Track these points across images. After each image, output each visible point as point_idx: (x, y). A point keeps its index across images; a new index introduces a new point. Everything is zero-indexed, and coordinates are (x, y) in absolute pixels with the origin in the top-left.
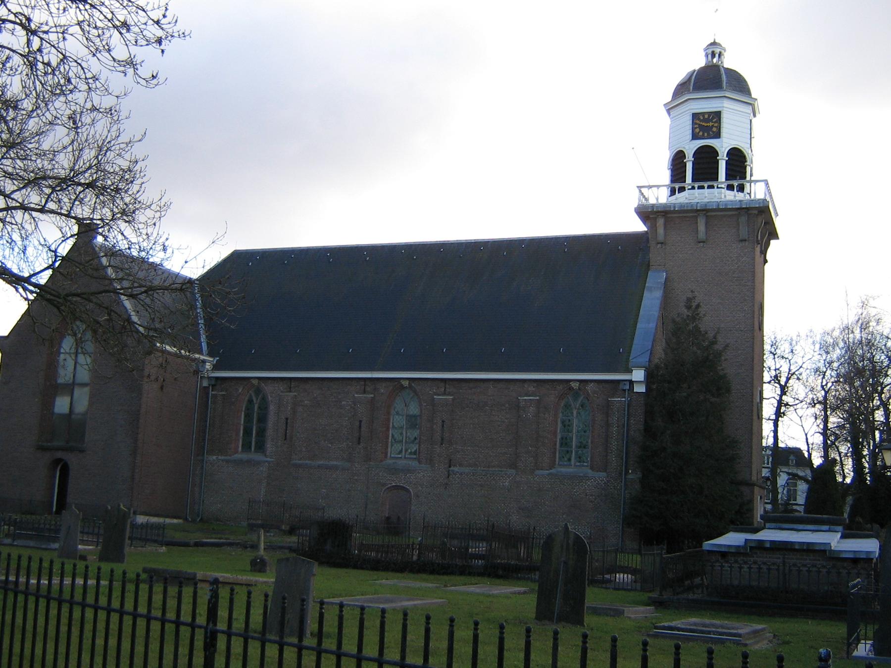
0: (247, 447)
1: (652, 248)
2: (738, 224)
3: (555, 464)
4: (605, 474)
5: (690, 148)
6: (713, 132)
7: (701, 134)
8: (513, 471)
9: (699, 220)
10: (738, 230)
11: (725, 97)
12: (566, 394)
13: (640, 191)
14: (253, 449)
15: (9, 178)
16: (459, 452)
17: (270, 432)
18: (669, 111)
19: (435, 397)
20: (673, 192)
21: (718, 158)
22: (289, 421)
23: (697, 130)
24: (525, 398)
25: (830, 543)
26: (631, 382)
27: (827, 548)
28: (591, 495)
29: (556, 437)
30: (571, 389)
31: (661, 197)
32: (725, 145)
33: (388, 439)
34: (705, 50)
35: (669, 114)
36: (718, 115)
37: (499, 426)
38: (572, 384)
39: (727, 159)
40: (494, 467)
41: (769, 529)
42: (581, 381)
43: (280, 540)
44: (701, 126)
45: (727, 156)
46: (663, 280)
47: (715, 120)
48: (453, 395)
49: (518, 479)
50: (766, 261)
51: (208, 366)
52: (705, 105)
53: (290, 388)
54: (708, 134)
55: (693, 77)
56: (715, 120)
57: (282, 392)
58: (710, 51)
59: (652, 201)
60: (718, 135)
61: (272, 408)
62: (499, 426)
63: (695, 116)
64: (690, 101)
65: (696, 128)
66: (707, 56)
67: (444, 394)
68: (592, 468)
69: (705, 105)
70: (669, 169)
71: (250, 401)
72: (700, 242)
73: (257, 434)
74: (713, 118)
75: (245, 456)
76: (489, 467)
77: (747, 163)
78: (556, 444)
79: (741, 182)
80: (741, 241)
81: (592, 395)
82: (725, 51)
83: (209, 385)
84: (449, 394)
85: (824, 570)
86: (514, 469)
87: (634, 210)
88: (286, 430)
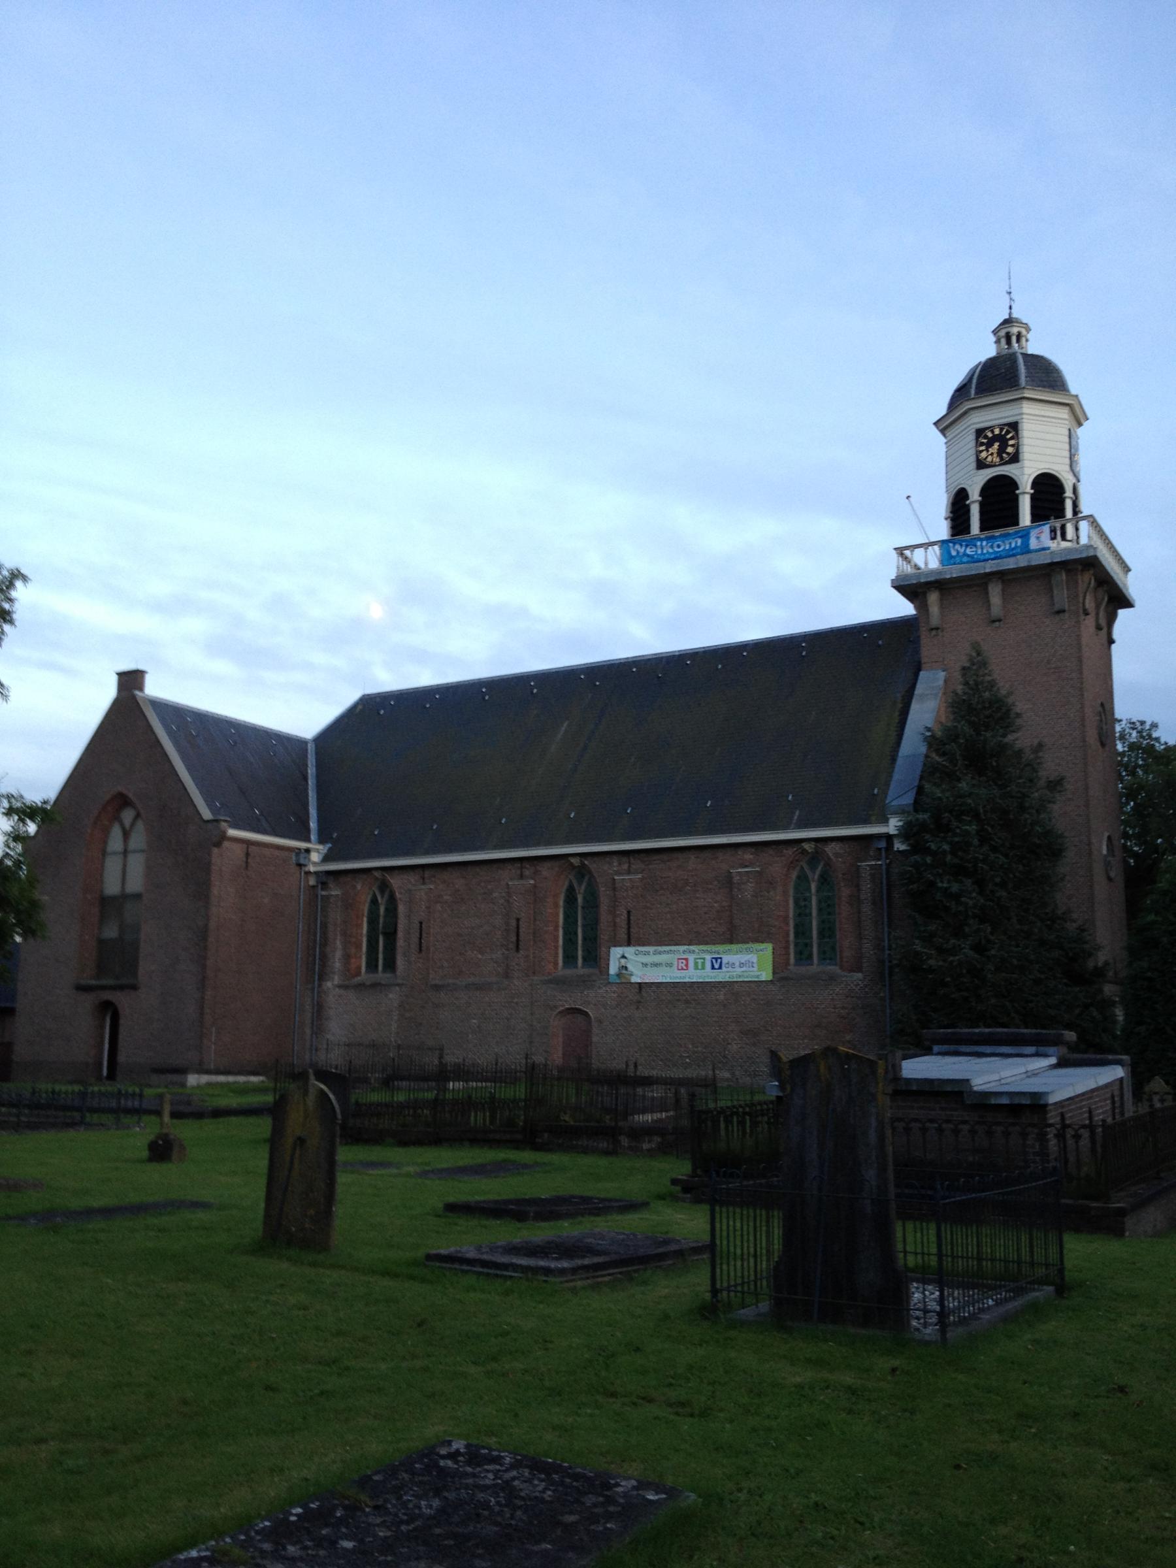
0: (372, 966)
1: (923, 637)
4: (860, 975)
5: (975, 484)
6: (1008, 454)
9: (990, 588)
12: (797, 861)
13: (902, 554)
14: (380, 968)
15: (1101, 721)
18: (943, 431)
21: (1017, 492)
22: (423, 926)
24: (740, 870)
25: (968, 1080)
28: (843, 1008)
29: (787, 924)
30: (804, 852)
31: (930, 561)
32: (1027, 471)
33: (558, 941)
35: (944, 435)
36: (1014, 426)
38: (806, 846)
39: (1032, 491)
41: (939, 1054)
43: (37, 1120)
45: (1032, 488)
46: (941, 682)
50: (1111, 641)
51: (315, 857)
52: (993, 417)
53: (423, 879)
58: (1002, 333)
60: (1015, 458)
61: (401, 908)
63: (980, 432)
64: (972, 412)
66: (998, 342)
67: (629, 872)
68: (841, 968)
69: (993, 417)
70: (946, 519)
71: (374, 901)
73: (821, 934)
74: (1008, 432)
78: (788, 935)
81: (834, 860)
82: (1028, 330)
83: (317, 882)
84: (636, 873)
85: (965, 1128)
87: (889, 584)
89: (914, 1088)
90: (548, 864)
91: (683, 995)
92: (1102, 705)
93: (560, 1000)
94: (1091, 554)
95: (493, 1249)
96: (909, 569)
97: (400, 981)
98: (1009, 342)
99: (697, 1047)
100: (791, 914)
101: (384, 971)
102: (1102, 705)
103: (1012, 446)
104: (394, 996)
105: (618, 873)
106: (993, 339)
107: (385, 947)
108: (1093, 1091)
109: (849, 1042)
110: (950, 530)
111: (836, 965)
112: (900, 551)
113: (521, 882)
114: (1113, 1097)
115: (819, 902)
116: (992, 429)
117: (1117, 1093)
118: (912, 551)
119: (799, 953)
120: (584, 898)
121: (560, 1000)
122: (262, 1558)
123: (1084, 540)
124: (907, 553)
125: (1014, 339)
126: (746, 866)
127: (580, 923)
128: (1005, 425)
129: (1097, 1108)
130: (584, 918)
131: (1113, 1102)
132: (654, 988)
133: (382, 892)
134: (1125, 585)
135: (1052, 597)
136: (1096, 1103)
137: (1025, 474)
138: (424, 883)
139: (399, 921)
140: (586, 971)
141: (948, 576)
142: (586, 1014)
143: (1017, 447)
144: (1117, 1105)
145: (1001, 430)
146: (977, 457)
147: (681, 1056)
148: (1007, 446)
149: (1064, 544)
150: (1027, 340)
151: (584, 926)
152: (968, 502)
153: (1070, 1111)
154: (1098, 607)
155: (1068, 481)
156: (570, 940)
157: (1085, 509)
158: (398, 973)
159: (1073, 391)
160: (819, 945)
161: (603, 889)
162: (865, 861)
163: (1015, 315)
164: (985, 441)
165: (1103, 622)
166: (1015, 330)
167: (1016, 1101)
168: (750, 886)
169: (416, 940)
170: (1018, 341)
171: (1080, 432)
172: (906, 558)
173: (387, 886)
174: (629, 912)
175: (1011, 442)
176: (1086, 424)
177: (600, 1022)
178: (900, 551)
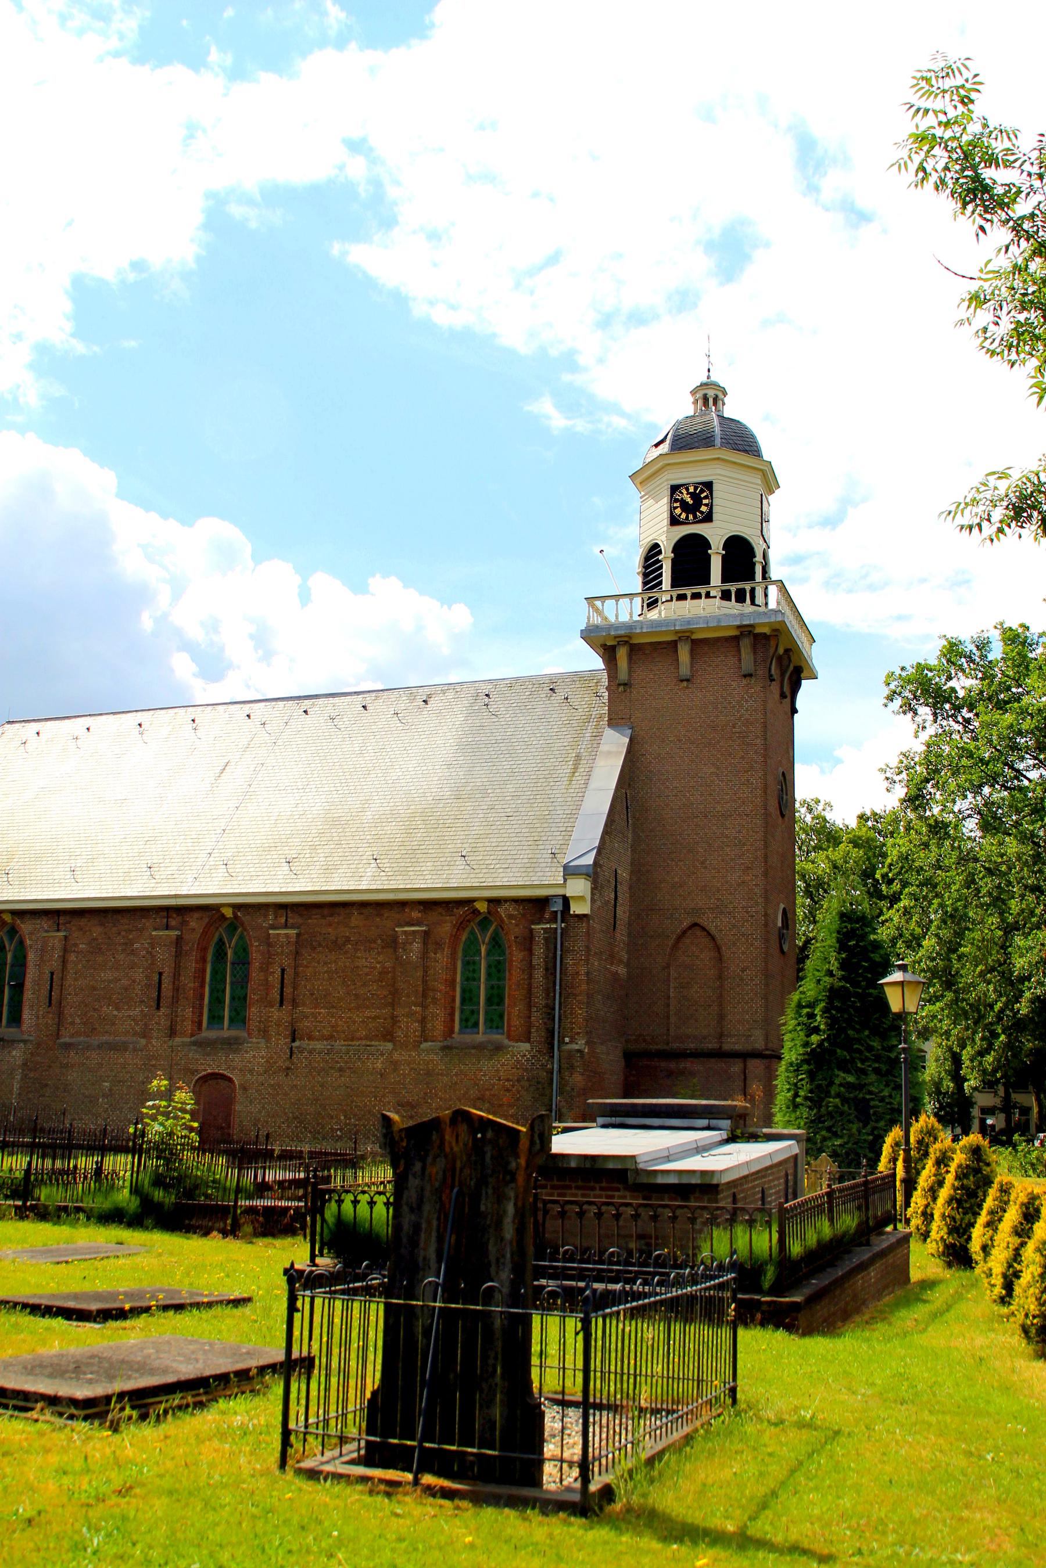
2: (739, 651)
4: (527, 1046)
5: (666, 538)
6: (702, 513)
7: (683, 516)
8: (389, 1046)
10: (740, 660)
11: (718, 459)
16: (307, 1017)
17: (28, 995)
19: (271, 932)
23: (678, 511)
27: (629, 1165)
28: (508, 1080)
29: (454, 990)
30: (476, 912)
34: (693, 393)
36: (709, 485)
40: (361, 1039)
44: (684, 505)
48: (298, 928)
49: (396, 1056)
50: (794, 711)
52: (691, 475)
53: (58, 925)
54: (695, 517)
57: (47, 931)
58: (699, 395)
59: (624, 618)
60: (708, 518)
61: (31, 957)
63: (674, 489)
65: (676, 508)
66: (696, 402)
67: (286, 926)
68: (509, 1037)
72: (682, 681)
73: (489, 1001)
74: (702, 491)
75: (212, 1034)
76: (352, 1040)
77: (756, 559)
78: (454, 1001)
80: (745, 676)
82: (725, 394)
84: (293, 927)
86: (389, 1041)
88: (51, 991)
90: (196, 915)
91: (337, 1062)
92: (783, 774)
93: (202, 1064)
94: (779, 619)
95: (36, 1367)
96: (597, 620)
97: (26, 1037)
99: (350, 1119)
100: (458, 979)
101: (9, 1025)
102: (783, 774)
103: (706, 505)
105: (274, 927)
106: (692, 399)
107: (11, 999)
108: (767, 1168)
109: (512, 1116)
111: (503, 1034)
113: (167, 932)
114: (787, 1175)
115: (489, 966)
117: (791, 1171)
119: (465, 1021)
120: (235, 953)
121: (202, 1064)
122: (853, 930)
123: (772, 605)
126: (413, 925)
127: (228, 981)
129: (770, 1188)
130: (233, 975)
131: (787, 1181)
132: (195, 923)
134: (810, 657)
136: (770, 1181)
137: (716, 534)
138: (58, 930)
139: (28, 971)
140: (234, 1033)
142: (230, 1080)
143: (710, 506)
144: (791, 1184)
145: (696, 488)
146: (671, 513)
147: (332, 1129)
148: (701, 504)
151: (232, 983)
153: (743, 1191)
154: (783, 675)
155: (759, 549)
157: (774, 574)
158: (25, 1027)
159: (766, 456)
160: (486, 1013)
161: (257, 944)
162: (538, 923)
165: (787, 690)
166: (711, 393)
167: (685, 1180)
168: (417, 946)
169: (46, 993)
170: (715, 403)
171: (771, 498)
172: (597, 610)
173: (17, 932)
175: (705, 501)
176: (777, 491)
177: (245, 1089)
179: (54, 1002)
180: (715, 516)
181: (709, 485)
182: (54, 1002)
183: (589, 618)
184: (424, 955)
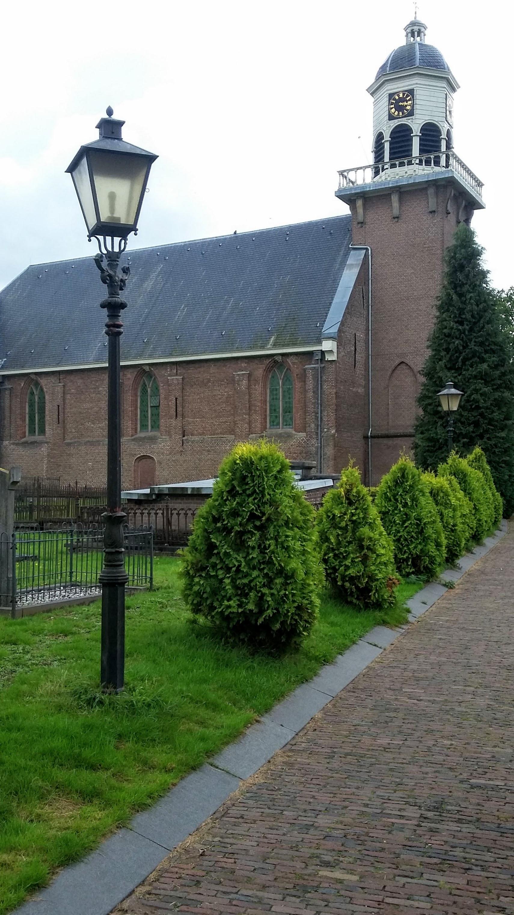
0: (32, 431)
3: (266, 428)
4: (304, 434)
7: (396, 113)
9: (392, 197)
11: (417, 73)
17: (47, 418)
18: (372, 94)
20: (377, 173)
26: (323, 353)
28: (295, 453)
29: (266, 405)
30: (276, 362)
34: (405, 29)
36: (411, 92)
37: (220, 399)
38: (276, 358)
42: (283, 355)
47: (409, 98)
55: (389, 62)
56: (409, 98)
58: (409, 30)
59: (360, 182)
60: (411, 113)
62: (220, 399)
63: (391, 96)
65: (392, 108)
70: (372, 152)
74: (407, 96)
78: (266, 411)
79: (437, 154)
89: (189, 492)
90: (131, 370)
93: (138, 451)
96: (344, 183)
98: (413, 36)
104: (44, 449)
110: (374, 159)
112: (342, 173)
116: (397, 93)
118: (348, 173)
119: (272, 422)
120: (152, 390)
121: (138, 451)
124: (345, 174)
125: (416, 33)
128: (406, 91)
133: (37, 388)
135: (428, 203)
141: (368, 189)
143: (413, 106)
145: (404, 94)
149: (437, 169)
150: (425, 35)
152: (383, 141)
155: (444, 128)
156: (144, 415)
158: (47, 436)
163: (418, 19)
164: (394, 102)
166: (416, 28)
174: (176, 399)
178: (342, 173)
179: (60, 421)
180: (416, 112)
181: (411, 92)
182: (60, 421)
183: (340, 184)
184: (249, 387)
